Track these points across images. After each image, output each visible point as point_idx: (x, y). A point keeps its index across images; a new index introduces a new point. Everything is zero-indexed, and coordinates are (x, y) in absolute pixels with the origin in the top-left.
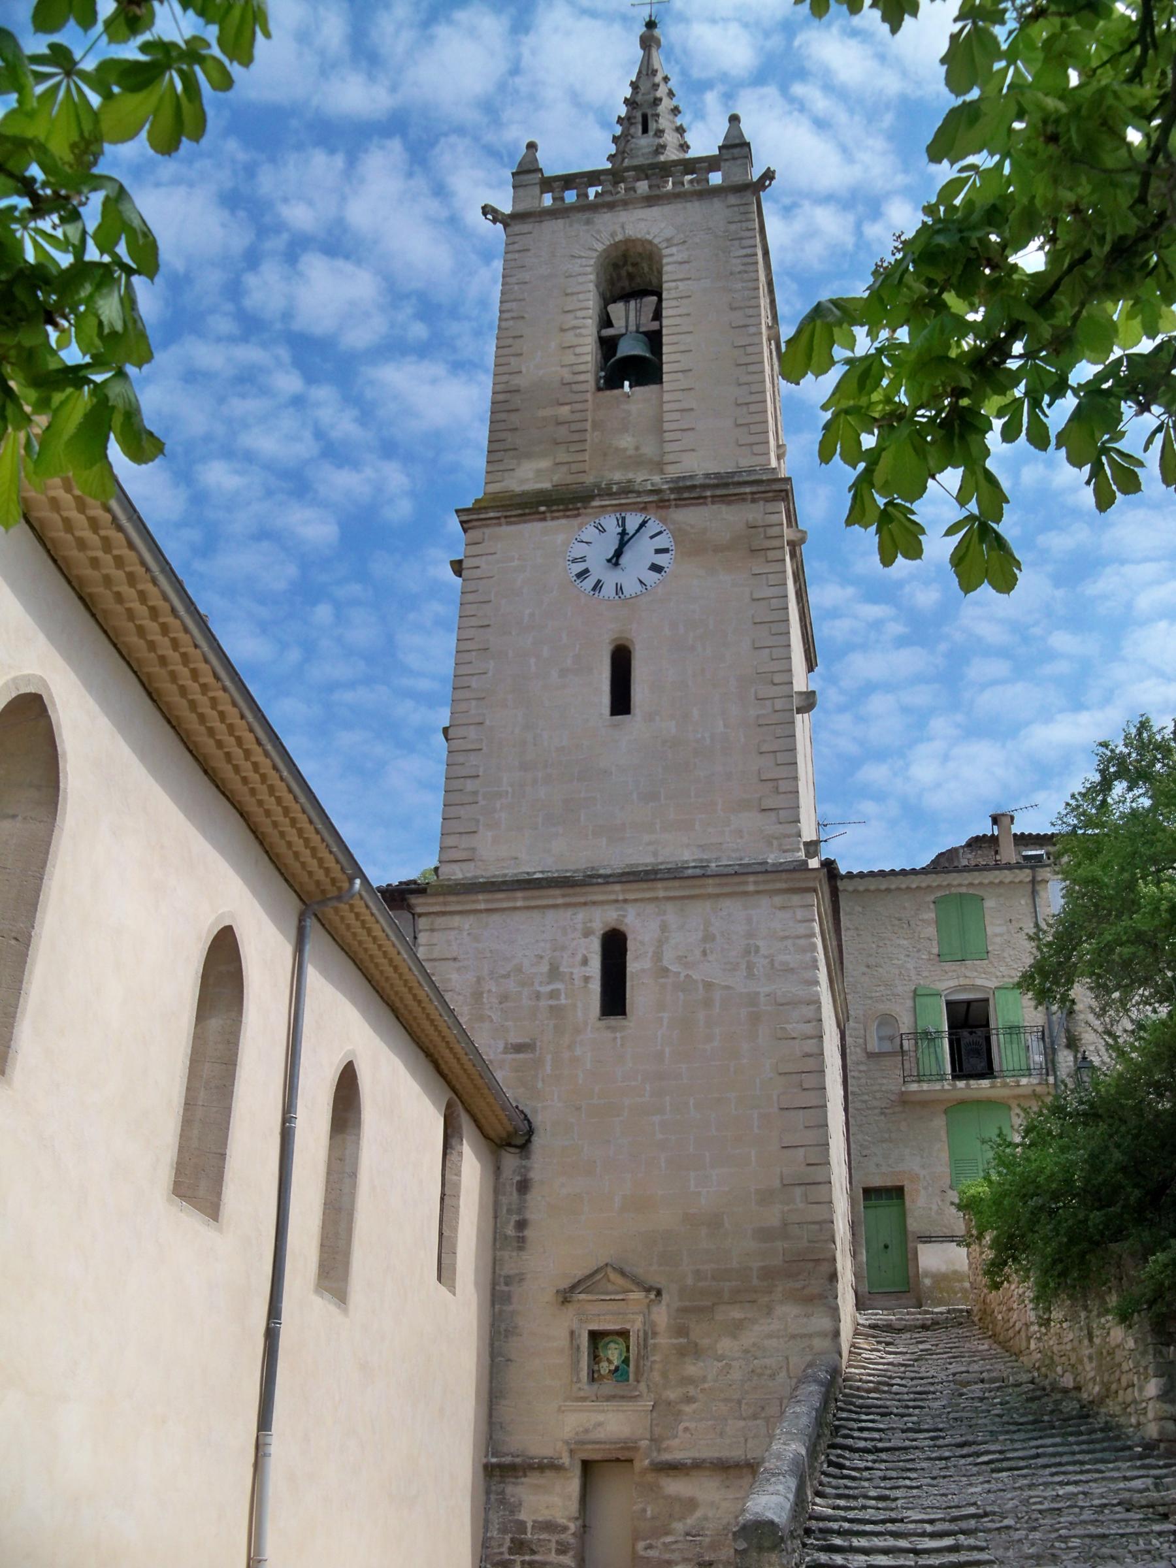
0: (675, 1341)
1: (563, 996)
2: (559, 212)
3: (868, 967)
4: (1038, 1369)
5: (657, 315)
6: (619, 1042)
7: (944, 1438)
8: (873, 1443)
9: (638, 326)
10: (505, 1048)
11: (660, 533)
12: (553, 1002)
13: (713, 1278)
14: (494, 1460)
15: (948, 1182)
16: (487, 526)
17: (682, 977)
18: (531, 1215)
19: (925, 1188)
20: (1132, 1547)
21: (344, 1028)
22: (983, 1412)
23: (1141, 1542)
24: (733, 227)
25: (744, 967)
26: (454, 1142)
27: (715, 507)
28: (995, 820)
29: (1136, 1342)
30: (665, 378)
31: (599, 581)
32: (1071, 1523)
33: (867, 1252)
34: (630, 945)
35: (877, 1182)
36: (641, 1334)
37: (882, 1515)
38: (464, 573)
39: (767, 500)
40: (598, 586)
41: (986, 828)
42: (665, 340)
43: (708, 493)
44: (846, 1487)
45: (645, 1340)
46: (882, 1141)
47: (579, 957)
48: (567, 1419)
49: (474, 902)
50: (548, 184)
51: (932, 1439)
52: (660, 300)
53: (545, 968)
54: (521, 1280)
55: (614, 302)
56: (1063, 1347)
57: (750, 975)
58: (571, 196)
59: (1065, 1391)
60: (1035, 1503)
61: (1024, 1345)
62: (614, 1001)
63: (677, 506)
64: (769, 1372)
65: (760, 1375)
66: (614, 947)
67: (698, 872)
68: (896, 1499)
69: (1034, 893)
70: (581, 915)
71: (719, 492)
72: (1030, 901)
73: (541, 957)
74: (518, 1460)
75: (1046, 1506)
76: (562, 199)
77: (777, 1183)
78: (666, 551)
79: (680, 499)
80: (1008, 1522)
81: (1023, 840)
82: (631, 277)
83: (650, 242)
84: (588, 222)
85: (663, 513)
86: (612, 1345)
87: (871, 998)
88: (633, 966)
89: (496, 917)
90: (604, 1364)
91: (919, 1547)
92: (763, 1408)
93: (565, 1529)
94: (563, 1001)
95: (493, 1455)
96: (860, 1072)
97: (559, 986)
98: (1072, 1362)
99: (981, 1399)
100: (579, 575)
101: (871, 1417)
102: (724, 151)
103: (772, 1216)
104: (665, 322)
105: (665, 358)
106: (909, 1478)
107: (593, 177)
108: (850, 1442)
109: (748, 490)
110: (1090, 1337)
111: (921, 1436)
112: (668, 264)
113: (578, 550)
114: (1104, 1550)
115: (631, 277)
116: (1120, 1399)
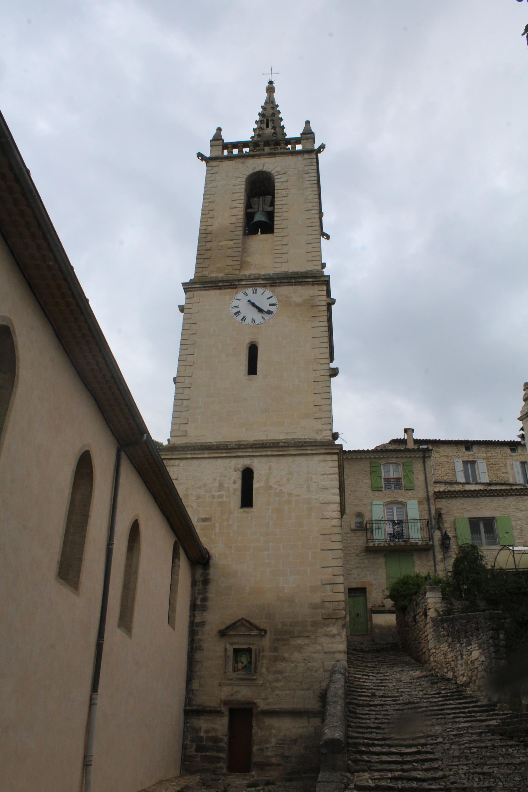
0: (272, 654)
1: (225, 497)
2: (231, 157)
3: (352, 491)
4: (435, 669)
5: (272, 204)
6: (249, 518)
7: (398, 700)
8: (367, 702)
9: (263, 209)
10: (198, 520)
11: (271, 297)
12: (220, 500)
13: (290, 625)
14: (188, 708)
15: (386, 586)
16: (195, 291)
17: (278, 491)
18: (210, 595)
19: (376, 589)
20: (500, 752)
21: (136, 503)
22: (413, 689)
23: (504, 750)
24: (306, 168)
25: (306, 486)
26: (176, 561)
27: (296, 287)
28: (406, 431)
29: (485, 658)
30: (275, 231)
31: (244, 317)
32: (469, 741)
33: (350, 617)
34: (255, 475)
35: (354, 586)
36: (258, 651)
37: (380, 736)
38: (185, 311)
39: (318, 285)
40: (244, 318)
41: (402, 436)
42: (275, 214)
43: (293, 281)
44: (360, 723)
45: (259, 653)
46: (357, 568)
47: (232, 480)
48: (217, 690)
49: (186, 454)
50: (226, 146)
51: (393, 701)
52: (273, 197)
53: (217, 484)
54: (204, 625)
55: (253, 197)
56: (447, 660)
57: (309, 491)
58: (235, 151)
59: (448, 680)
60: (449, 731)
61: (427, 658)
62: (247, 500)
63: (279, 286)
64: (315, 669)
65: (310, 670)
66: (247, 475)
67: (286, 444)
68: (384, 729)
69: (424, 462)
70: (234, 461)
71: (298, 280)
72: (422, 465)
73: (215, 480)
74: (200, 708)
75: (455, 733)
76: (232, 152)
77: (319, 583)
78: (274, 305)
79: (281, 283)
80: (440, 740)
81: (417, 442)
82: (261, 188)
83: (270, 173)
84: (243, 163)
85: (273, 288)
86: (244, 656)
87: (353, 505)
88: (256, 485)
89: (195, 461)
90: (240, 664)
91: (402, 752)
92: (312, 686)
93: (221, 740)
94: (225, 499)
95: (189, 706)
96: (348, 537)
97: (223, 493)
98: (452, 666)
99: (411, 683)
100: (236, 314)
101: (363, 690)
102: (303, 136)
103: (317, 598)
104: (276, 207)
105: (275, 222)
106: (387, 719)
107: (245, 144)
108: (357, 702)
109: (311, 280)
110: (462, 655)
111: (389, 699)
112: (278, 182)
113: (235, 303)
114: (488, 754)
115: (261, 188)
116: (477, 684)
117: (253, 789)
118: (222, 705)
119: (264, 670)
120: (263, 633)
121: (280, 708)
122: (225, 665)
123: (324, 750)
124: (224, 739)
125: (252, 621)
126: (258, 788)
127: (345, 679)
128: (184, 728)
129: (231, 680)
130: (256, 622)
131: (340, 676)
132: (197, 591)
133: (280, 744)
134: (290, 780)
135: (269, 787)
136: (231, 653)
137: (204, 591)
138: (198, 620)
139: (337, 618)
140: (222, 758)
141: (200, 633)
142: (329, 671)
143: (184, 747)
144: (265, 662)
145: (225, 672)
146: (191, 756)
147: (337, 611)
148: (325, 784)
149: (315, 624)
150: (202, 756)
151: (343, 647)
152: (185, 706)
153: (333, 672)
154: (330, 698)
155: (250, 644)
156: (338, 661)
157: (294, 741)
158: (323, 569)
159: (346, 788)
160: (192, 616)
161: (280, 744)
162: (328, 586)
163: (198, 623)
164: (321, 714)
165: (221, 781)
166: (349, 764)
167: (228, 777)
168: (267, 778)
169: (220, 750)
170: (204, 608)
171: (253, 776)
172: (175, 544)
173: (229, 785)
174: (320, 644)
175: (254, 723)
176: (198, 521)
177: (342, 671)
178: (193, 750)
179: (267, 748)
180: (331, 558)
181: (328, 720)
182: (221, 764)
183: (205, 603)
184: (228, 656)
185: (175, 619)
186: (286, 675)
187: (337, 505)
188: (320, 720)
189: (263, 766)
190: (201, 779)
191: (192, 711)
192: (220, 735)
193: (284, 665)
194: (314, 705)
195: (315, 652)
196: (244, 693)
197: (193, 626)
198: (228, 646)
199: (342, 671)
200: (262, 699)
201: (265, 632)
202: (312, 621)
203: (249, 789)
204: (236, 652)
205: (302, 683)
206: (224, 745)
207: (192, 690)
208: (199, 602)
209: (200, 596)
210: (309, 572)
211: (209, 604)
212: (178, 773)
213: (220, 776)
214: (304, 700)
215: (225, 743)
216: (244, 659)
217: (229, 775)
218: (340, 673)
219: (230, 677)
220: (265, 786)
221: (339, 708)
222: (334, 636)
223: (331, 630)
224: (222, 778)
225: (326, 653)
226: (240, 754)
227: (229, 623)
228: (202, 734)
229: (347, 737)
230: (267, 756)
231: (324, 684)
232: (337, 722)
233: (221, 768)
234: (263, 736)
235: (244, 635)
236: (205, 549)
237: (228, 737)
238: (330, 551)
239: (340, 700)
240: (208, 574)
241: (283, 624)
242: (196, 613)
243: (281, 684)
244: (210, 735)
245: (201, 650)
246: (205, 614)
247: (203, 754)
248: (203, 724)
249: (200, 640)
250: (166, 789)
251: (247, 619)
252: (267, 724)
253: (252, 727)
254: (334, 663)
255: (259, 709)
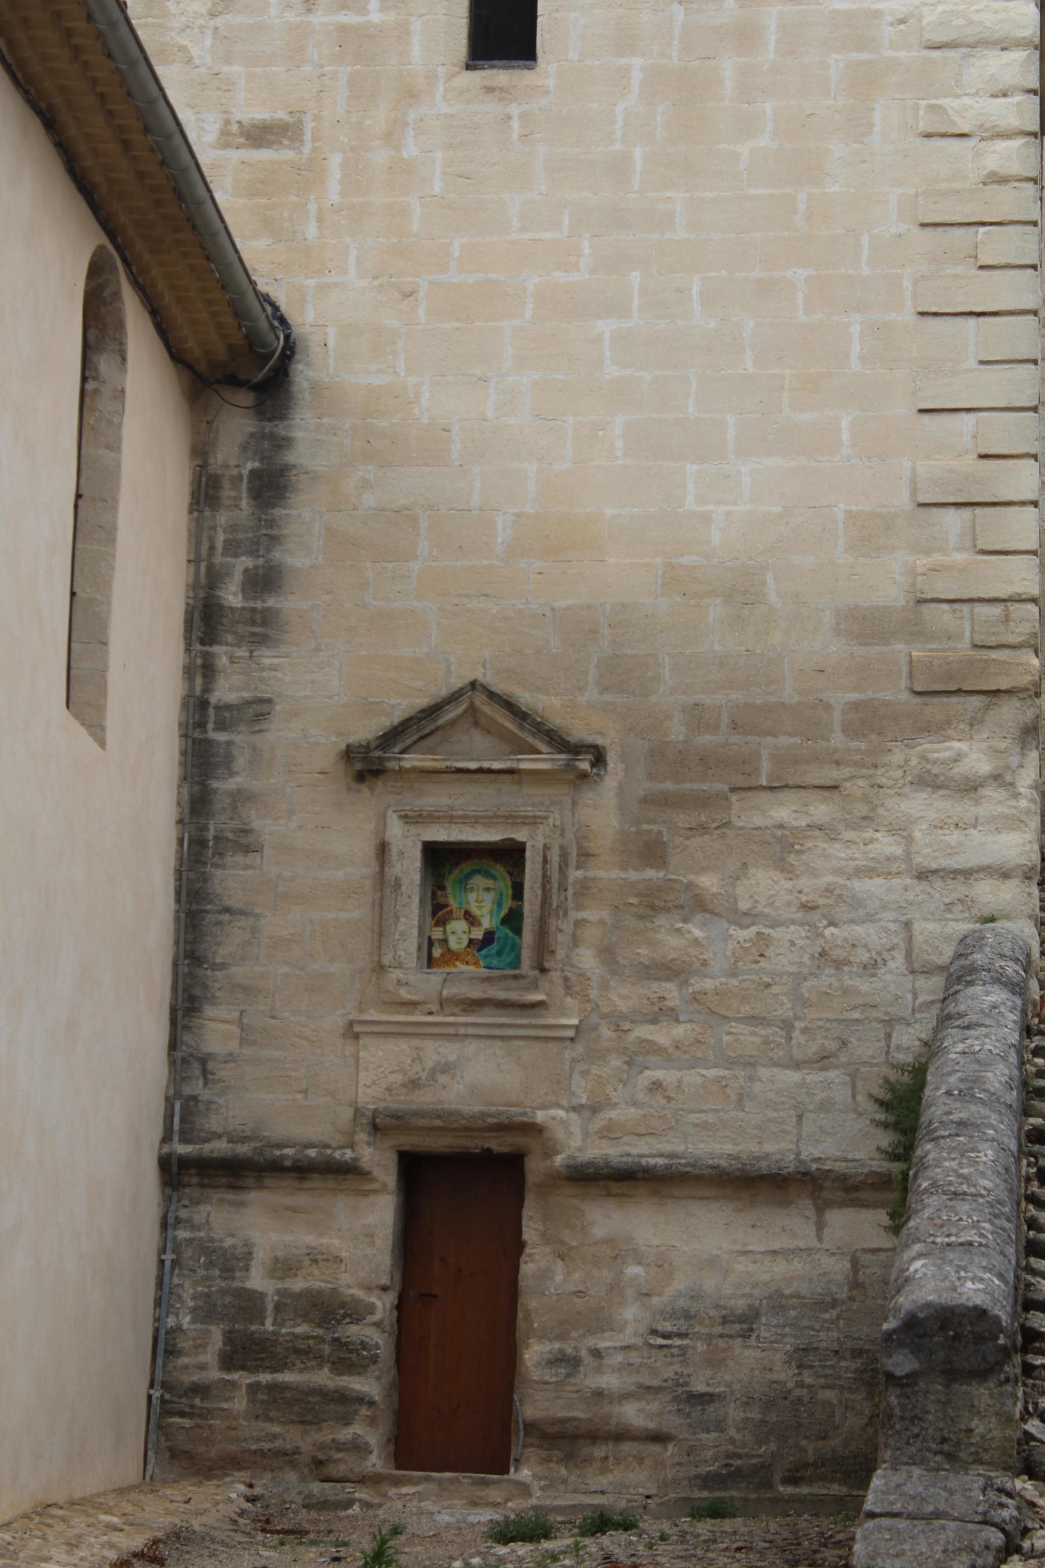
0: (633, 875)
6: (515, 124)
10: (225, 132)
13: (734, 726)
14: (183, 1149)
18: (293, 558)
26: (104, 364)
36: (555, 857)
54: (261, 717)
64: (864, 956)
65: (839, 964)
74: (243, 1149)
77: (903, 500)
86: (479, 881)
93: (355, 1312)
95: (185, 1140)
103: (886, 581)
117: (522, 1549)
118: (362, 1137)
119: (587, 959)
120: (585, 766)
121: (672, 1156)
122: (380, 933)
123: (902, 1363)
124: (371, 1309)
125: (524, 698)
126: (546, 1545)
127: (1024, 1013)
128: (163, 1250)
129: (411, 1005)
130: (547, 704)
131: (998, 995)
132: (220, 538)
133: (665, 1336)
134: (716, 1511)
135: (605, 1540)
136: (409, 868)
137: (265, 536)
138: (227, 691)
139: (997, 693)
140: (361, 1400)
141: (241, 762)
142: (942, 968)
143: (164, 1346)
144: (591, 914)
145: (380, 968)
146: (200, 1390)
147: (994, 655)
148: (902, 1524)
149: (868, 721)
150: (254, 1389)
151: (1019, 846)
152: (167, 1138)
153: (959, 975)
154: (939, 1105)
155: (512, 819)
156: (992, 919)
157: (743, 1323)
158: (926, 418)
159: (1010, 1549)
160: (201, 670)
161: (665, 1336)
162: (951, 514)
163: (228, 707)
164: (891, 1189)
165: (356, 1507)
166: (1028, 1436)
167: (392, 1492)
168: (597, 1500)
169: (349, 1358)
170: (262, 629)
171: (524, 1489)
172: (96, 269)
173: (396, 1531)
174: (893, 830)
175: (530, 1233)
176: (225, 140)
177: (1011, 969)
178: (210, 1356)
179: (596, 1353)
180: (972, 363)
181: (927, 1213)
182: (357, 1429)
183: (271, 602)
184: (398, 884)
185: (103, 689)
186: (709, 984)
187: (1019, 56)
188: (885, 1220)
189: (566, 1441)
190: (252, 1500)
191: (200, 1167)
192: (349, 1285)
193: (697, 933)
194: (851, 1141)
195: (868, 872)
196: (476, 1077)
197: (202, 725)
198: (395, 829)
199: (1011, 969)
200: (576, 1109)
201: (599, 758)
202: (856, 706)
203: (502, 1550)
204: (441, 860)
205: (787, 1026)
206: (374, 1333)
207: (203, 1061)
208: (232, 596)
209: (245, 562)
210: (845, 437)
211: (289, 603)
212: (130, 1470)
213: (349, 1488)
214: (800, 1117)
215: (377, 1324)
216: (482, 901)
217: (398, 1482)
218: (1000, 980)
219: (405, 994)
220: (583, 1534)
221: (988, 1154)
222: (970, 787)
223: (958, 758)
224: (362, 1494)
225: (923, 875)
226: (456, 1386)
227: (402, 705)
228: (258, 1280)
229: (1028, 1303)
230: (599, 1394)
231: (908, 1039)
232: (975, 1225)
233: (358, 1447)
234: (579, 1293)
235: (480, 771)
236: (266, 299)
237: (390, 1299)
238: (972, 321)
239: (994, 1118)
240: (282, 443)
241: (698, 716)
242: (221, 654)
243: (679, 1031)
244: (298, 1285)
245: (247, 849)
246: (267, 657)
247: (265, 1378)
248: (263, 1233)
249: (241, 797)
250: (72, 1545)
251: (499, 686)
252: (599, 1232)
253: (520, 1246)
254: (964, 927)
255: (559, 1160)
